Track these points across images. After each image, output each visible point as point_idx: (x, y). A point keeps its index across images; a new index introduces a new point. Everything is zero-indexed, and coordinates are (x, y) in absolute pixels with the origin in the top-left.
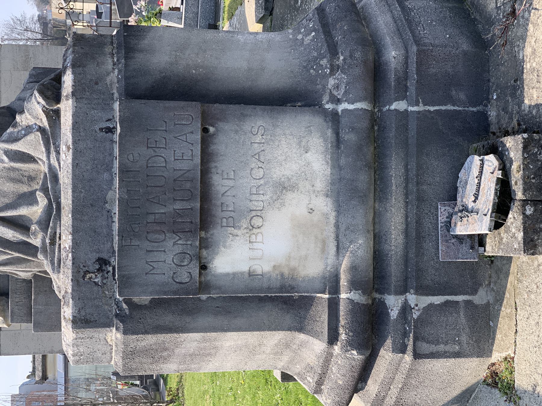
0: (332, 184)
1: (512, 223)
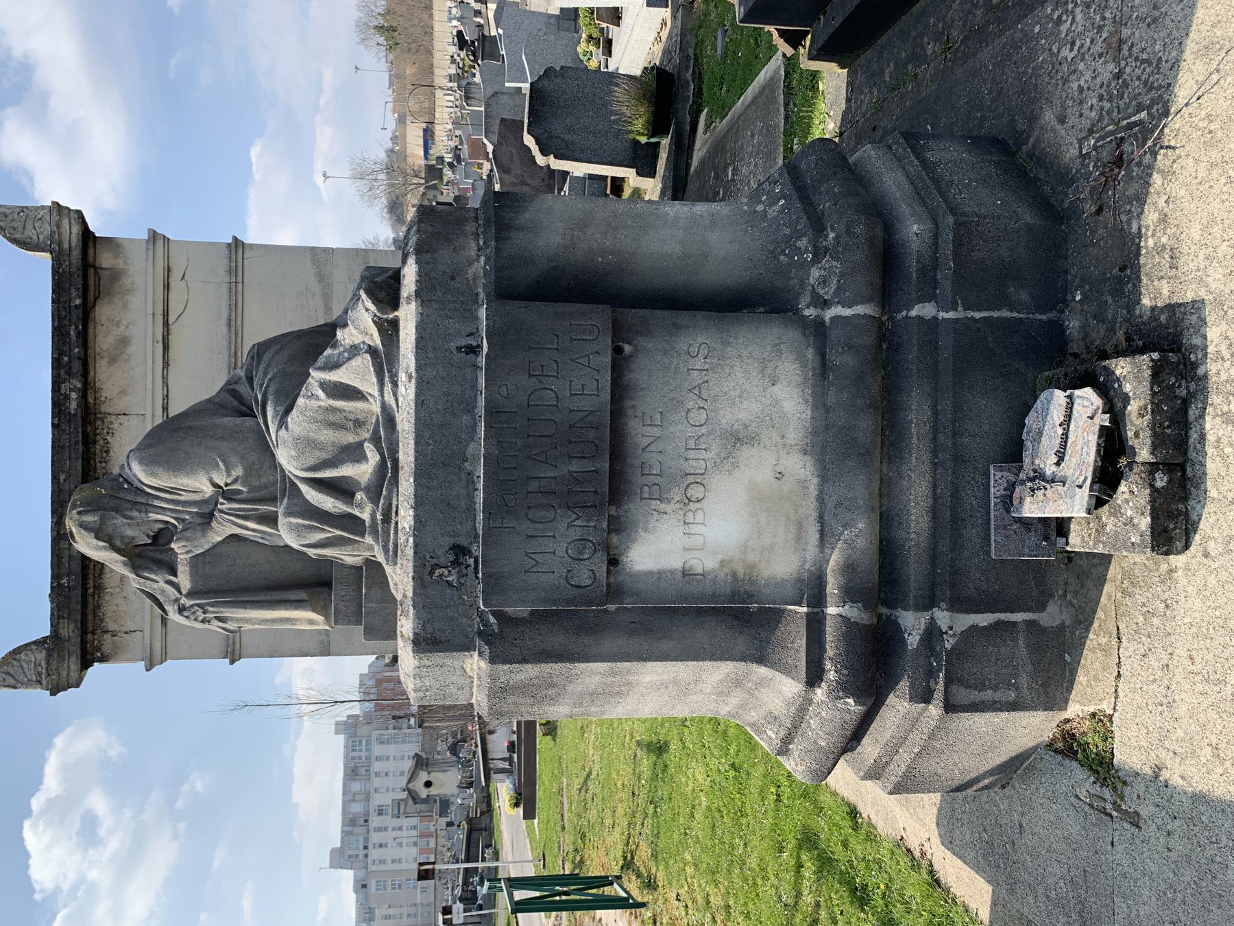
0: (814, 434)
1: (1127, 501)
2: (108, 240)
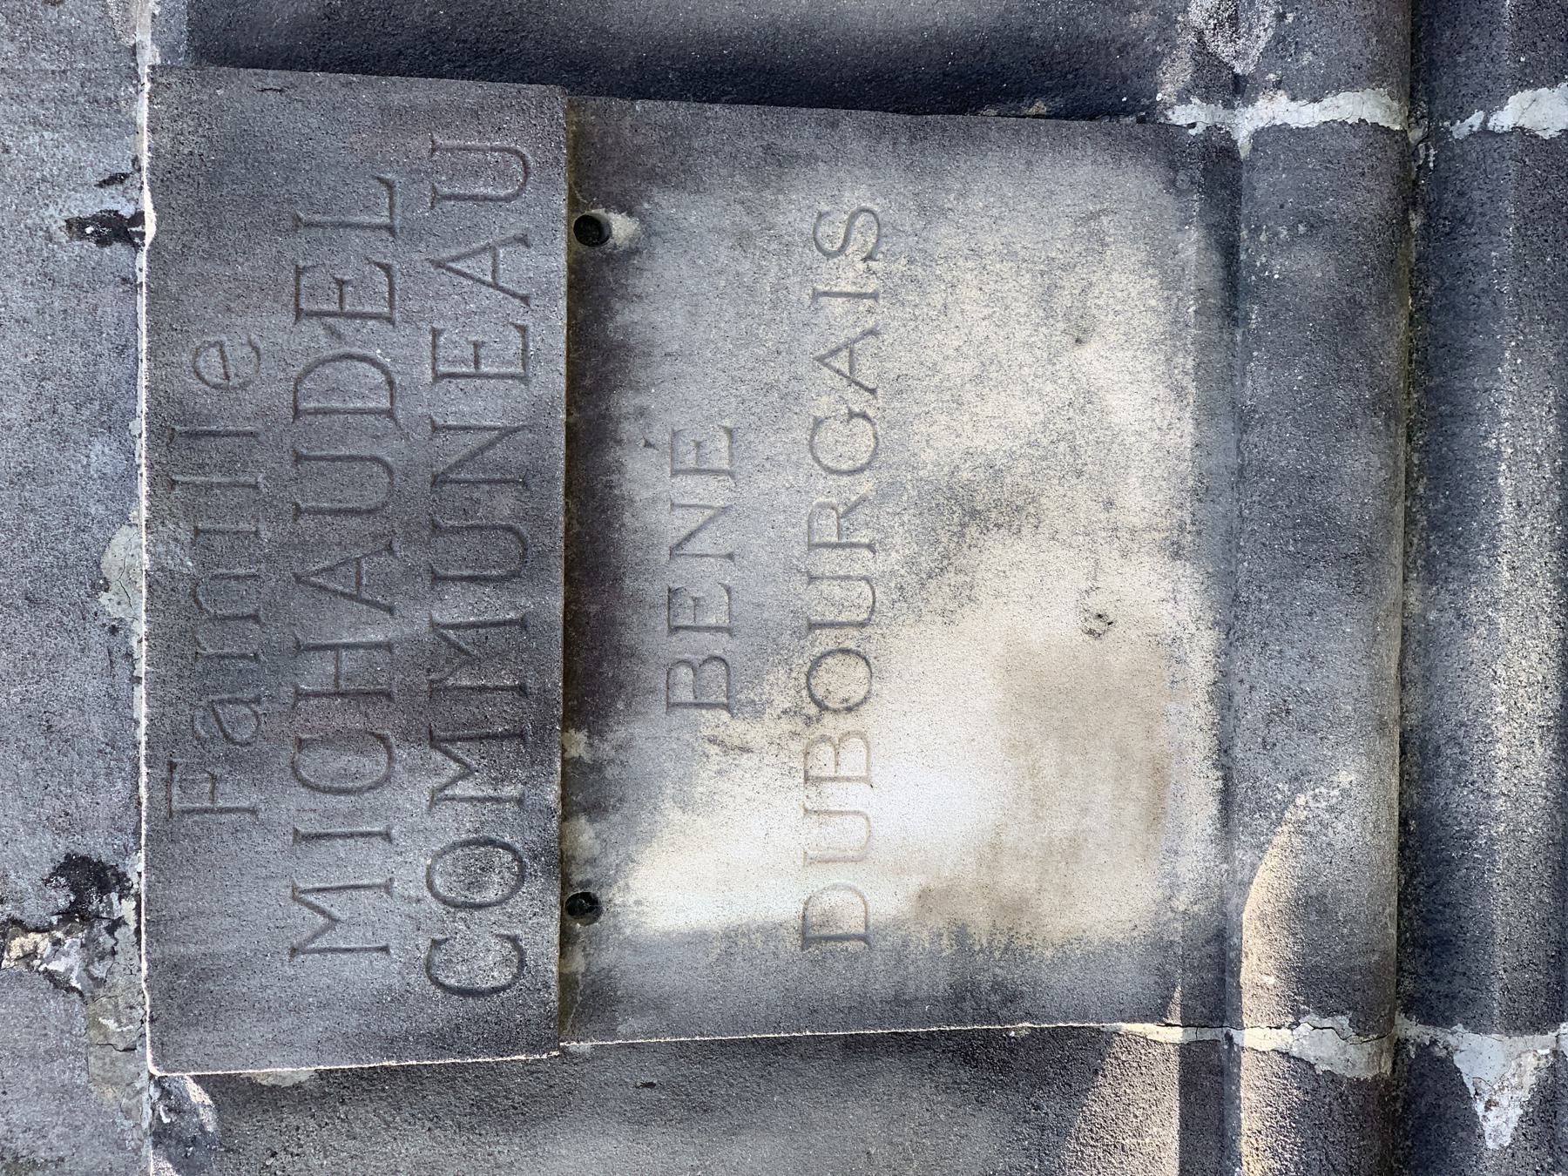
0: (1203, 493)
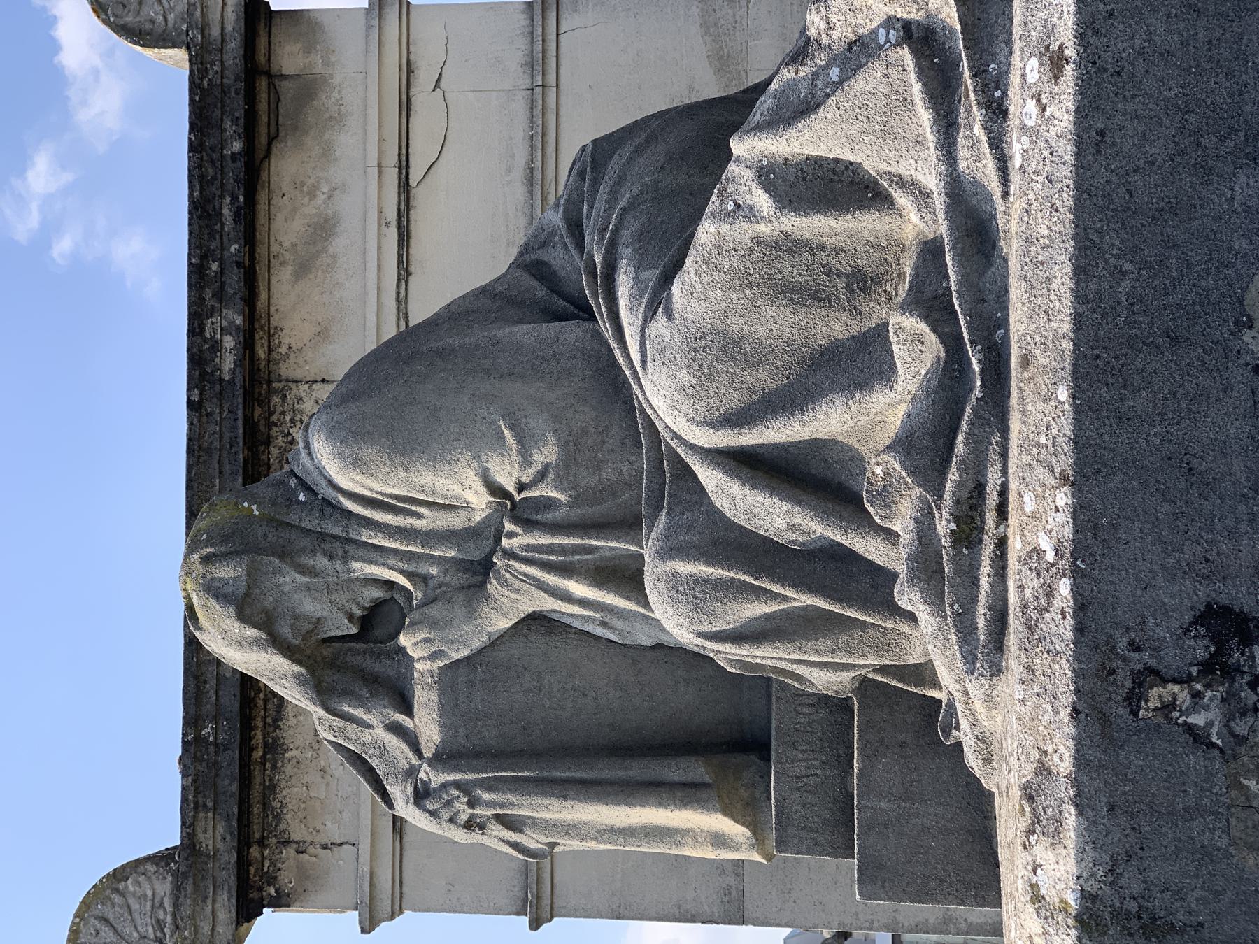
2: (294, 17)
